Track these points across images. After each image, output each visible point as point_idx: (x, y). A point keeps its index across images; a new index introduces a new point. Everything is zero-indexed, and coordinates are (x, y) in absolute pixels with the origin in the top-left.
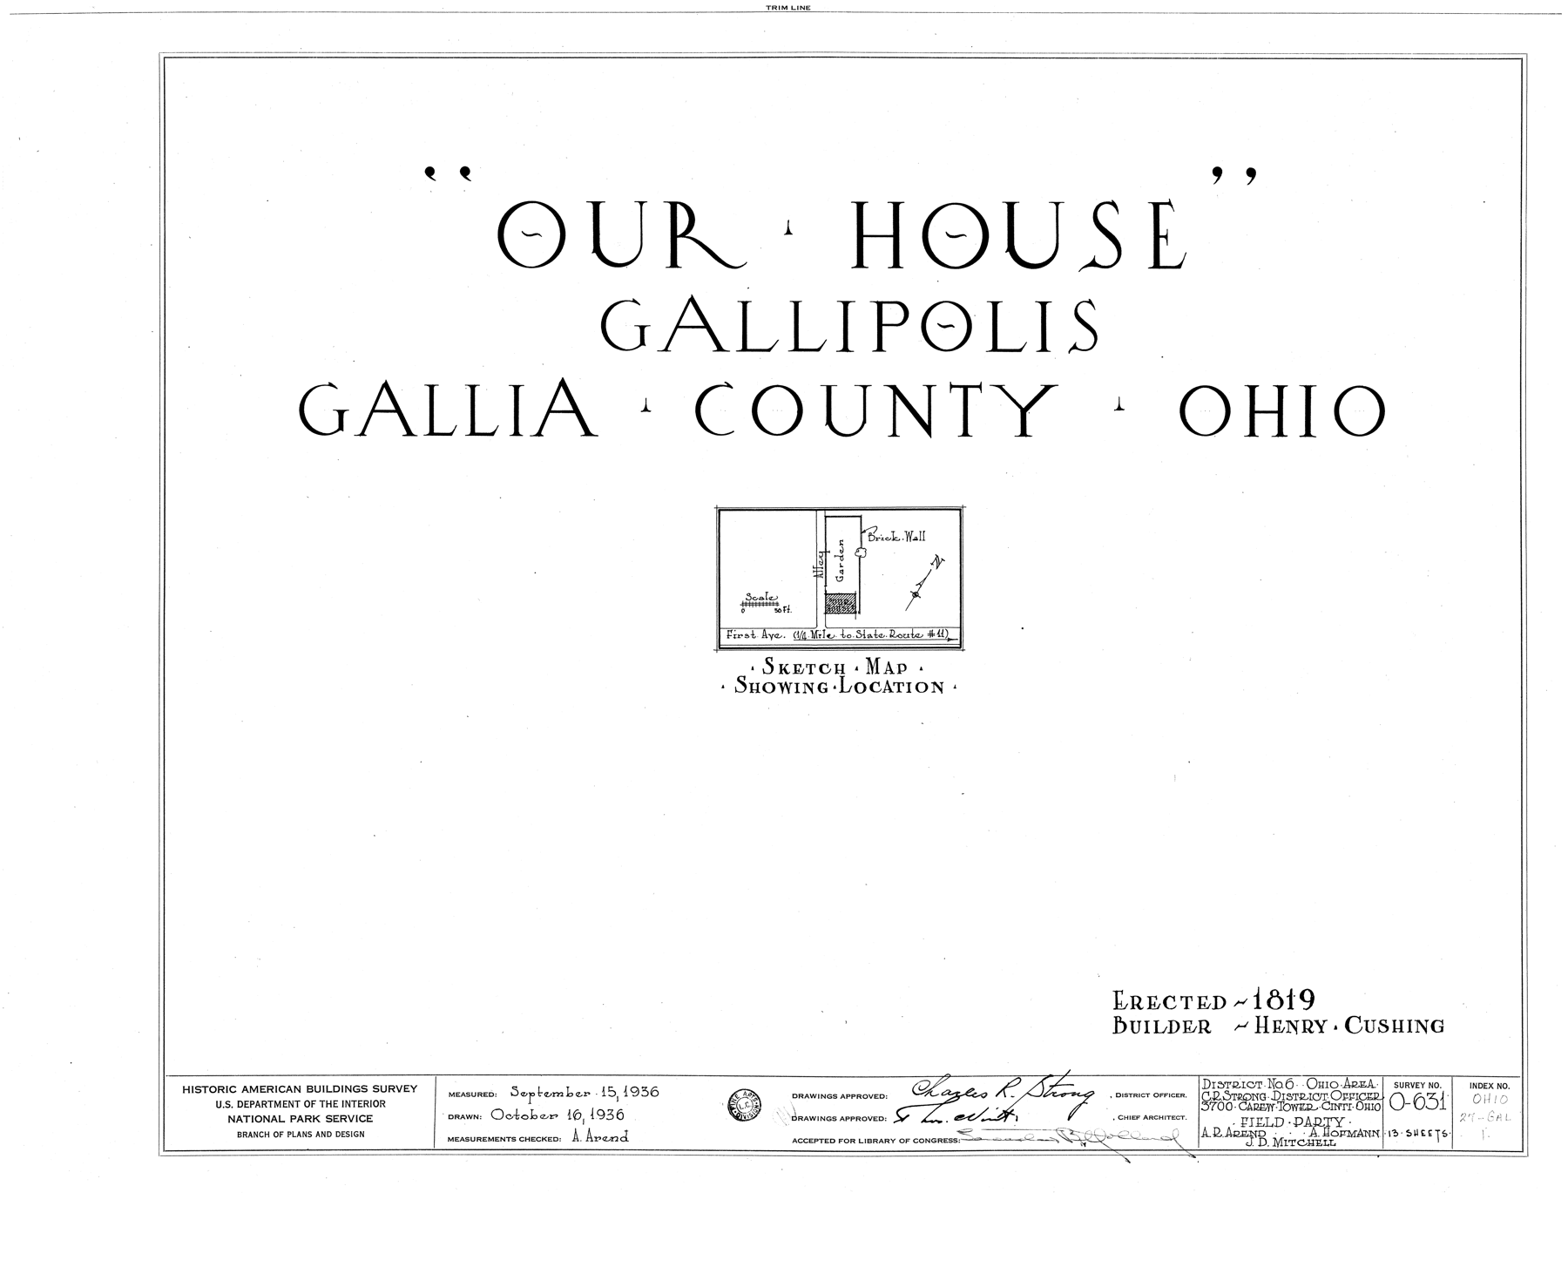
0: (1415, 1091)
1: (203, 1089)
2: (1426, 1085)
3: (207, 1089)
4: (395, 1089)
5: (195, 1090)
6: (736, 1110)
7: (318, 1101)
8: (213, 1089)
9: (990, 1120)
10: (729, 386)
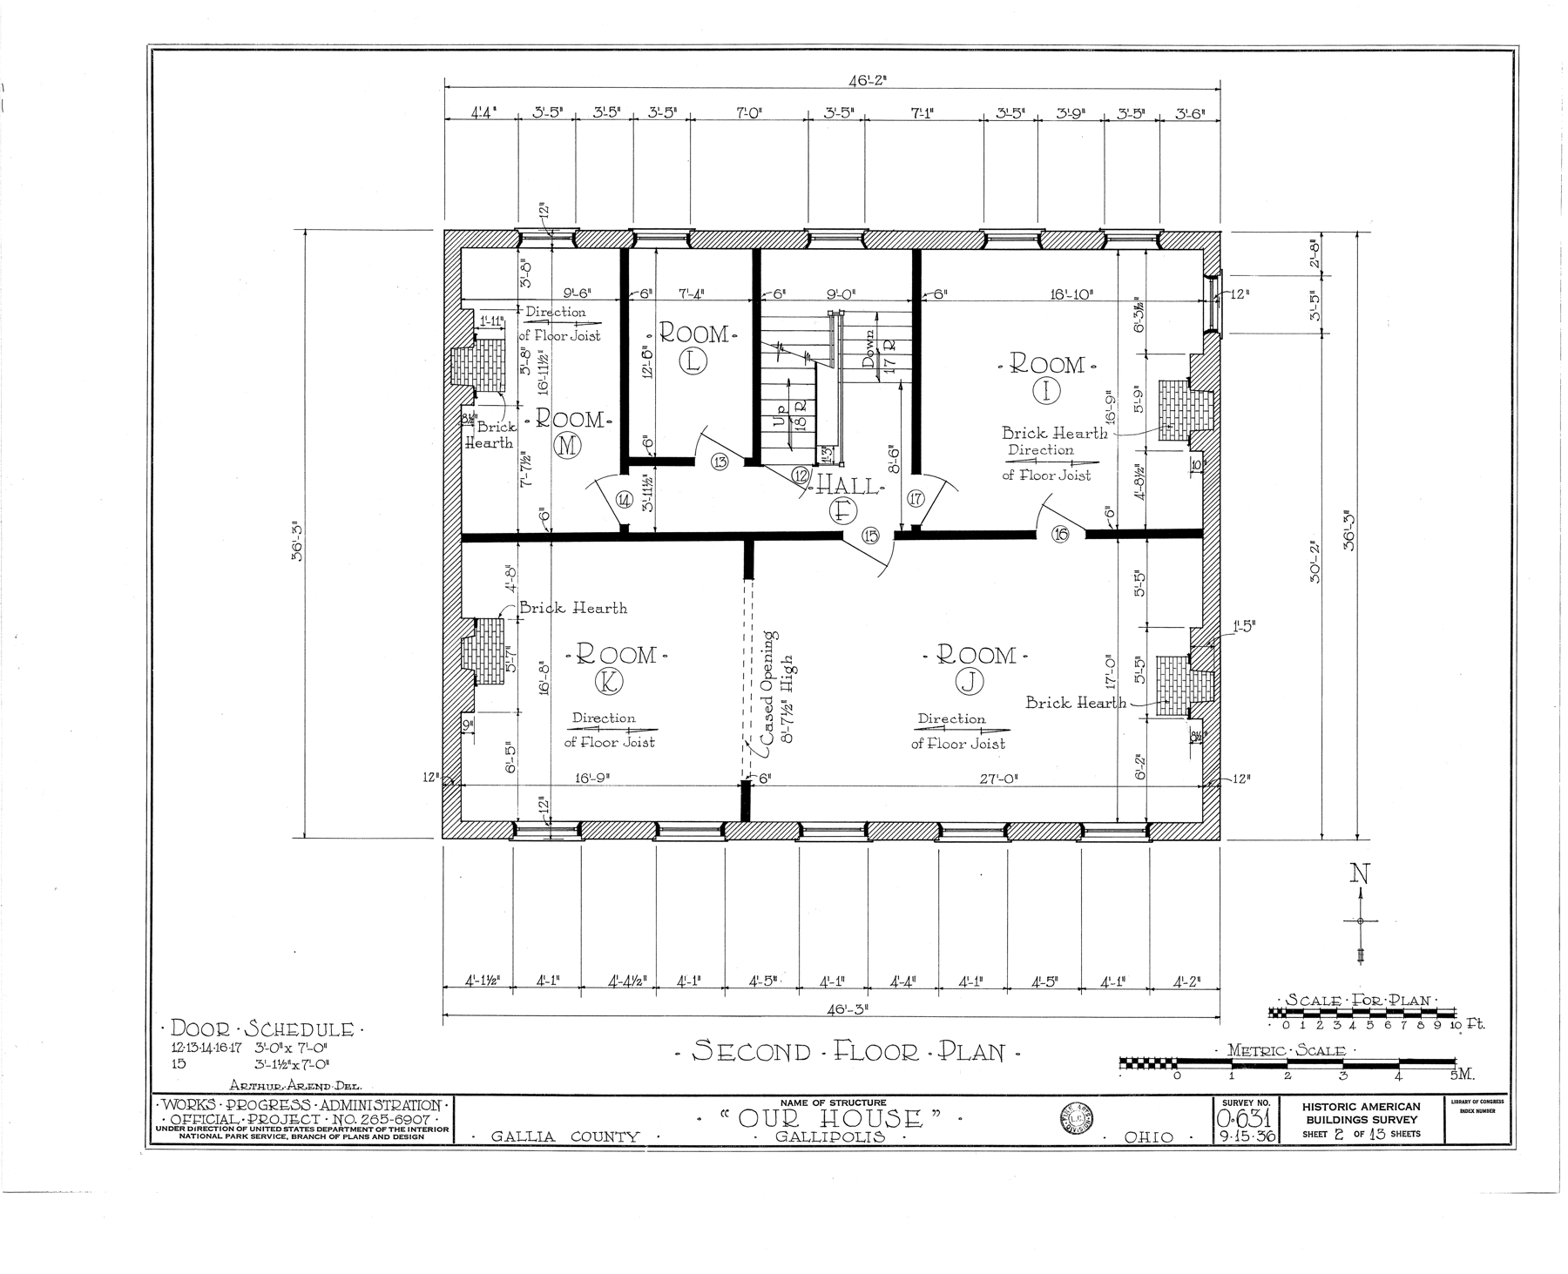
1: (1323, 1107)
2: (371, 1137)
4: (1396, 1120)
6: (1068, 1121)
8: (1333, 1107)
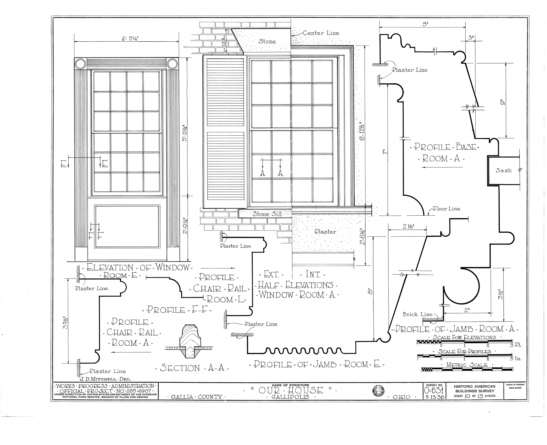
0: (432, 387)
1: (461, 386)
3: (463, 386)
4: (487, 391)
5: (458, 387)
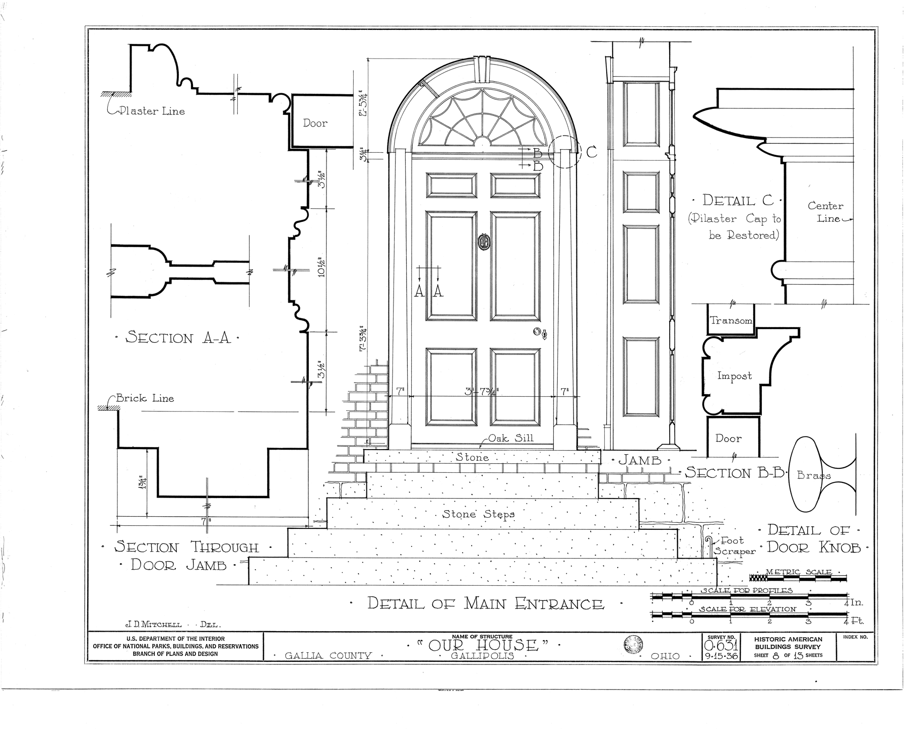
1: (766, 639)
4: (808, 647)
7: (186, 637)
8: (772, 639)
9: (149, 247)
10: (595, 147)
